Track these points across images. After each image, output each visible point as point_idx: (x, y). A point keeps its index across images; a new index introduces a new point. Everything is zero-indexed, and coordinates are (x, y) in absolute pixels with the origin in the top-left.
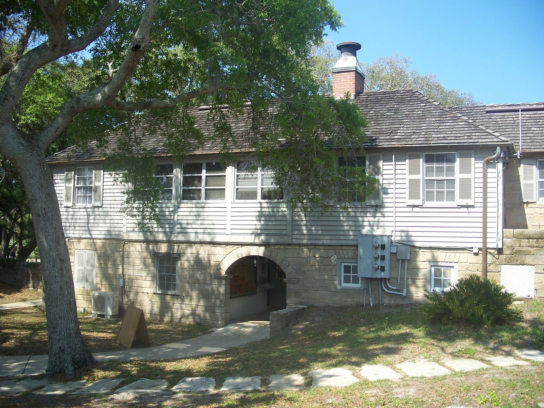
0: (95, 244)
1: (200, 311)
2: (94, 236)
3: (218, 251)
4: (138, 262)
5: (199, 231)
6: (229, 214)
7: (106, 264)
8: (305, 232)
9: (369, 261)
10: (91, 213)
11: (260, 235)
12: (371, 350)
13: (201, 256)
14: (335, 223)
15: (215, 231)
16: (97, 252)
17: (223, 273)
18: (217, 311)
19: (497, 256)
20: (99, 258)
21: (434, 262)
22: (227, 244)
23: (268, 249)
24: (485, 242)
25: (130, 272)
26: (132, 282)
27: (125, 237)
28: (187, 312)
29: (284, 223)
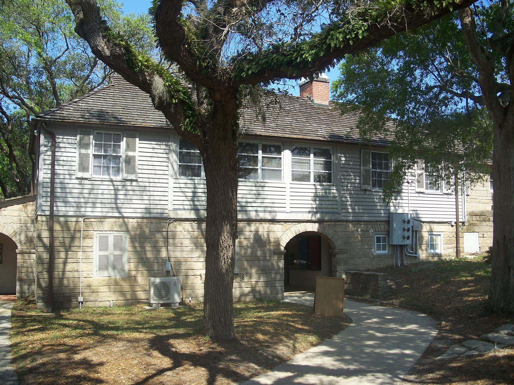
0: (126, 225)
1: (260, 287)
2: (125, 215)
3: (277, 227)
4: (187, 242)
5: (259, 209)
6: (288, 193)
7: (143, 247)
8: (350, 210)
9: (400, 232)
10: (120, 188)
11: (316, 213)
13: (260, 233)
14: (371, 204)
16: (130, 234)
17: (282, 249)
18: (277, 285)
20: (133, 239)
21: (431, 232)
22: (286, 221)
23: (322, 225)
24: (457, 218)
25: (177, 254)
26: (181, 264)
27: (172, 215)
28: (247, 290)
29: (335, 203)
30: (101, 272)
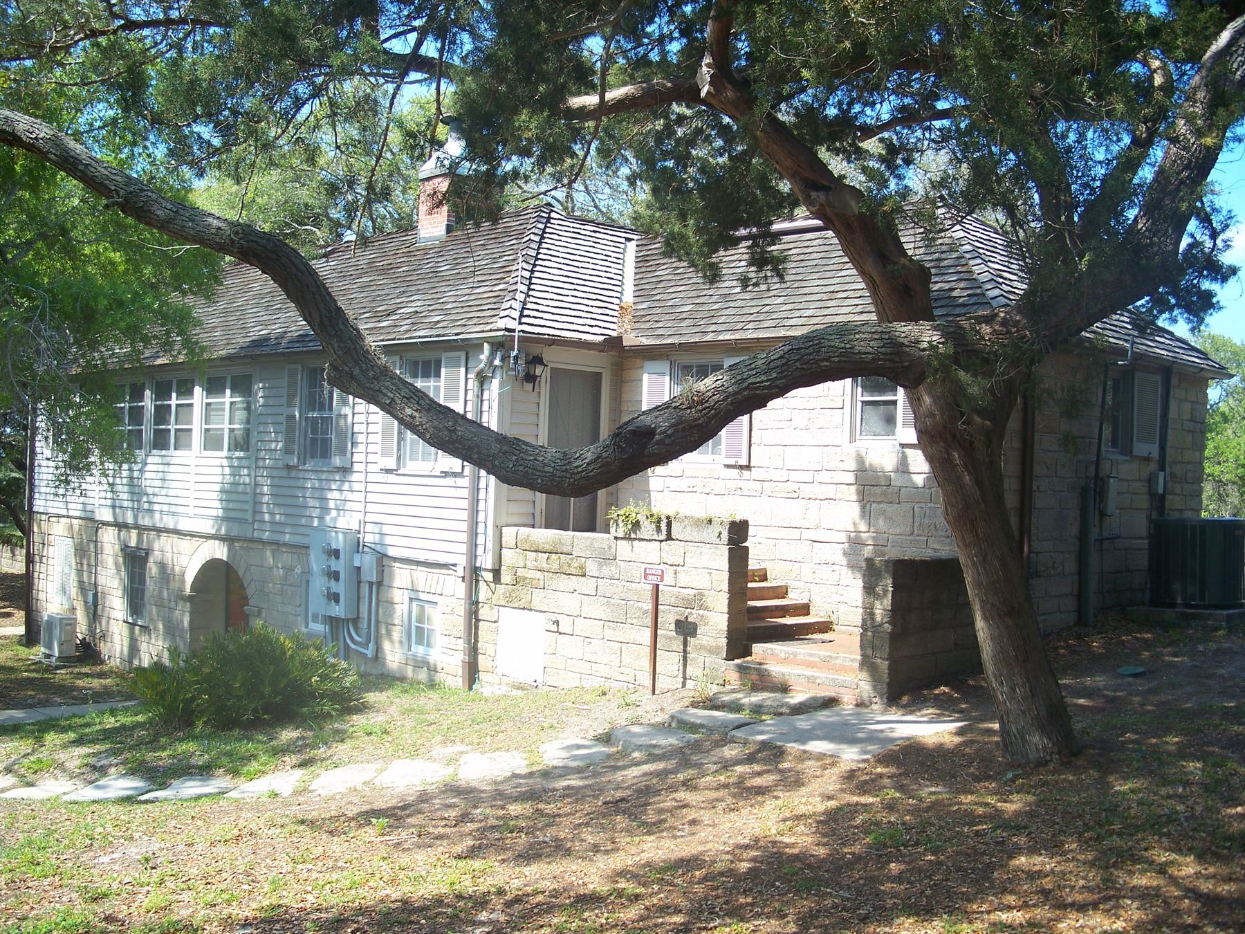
12: (1229, 879)
15: (180, 509)
19: (492, 585)
22: (192, 535)
30: (784, 584)
